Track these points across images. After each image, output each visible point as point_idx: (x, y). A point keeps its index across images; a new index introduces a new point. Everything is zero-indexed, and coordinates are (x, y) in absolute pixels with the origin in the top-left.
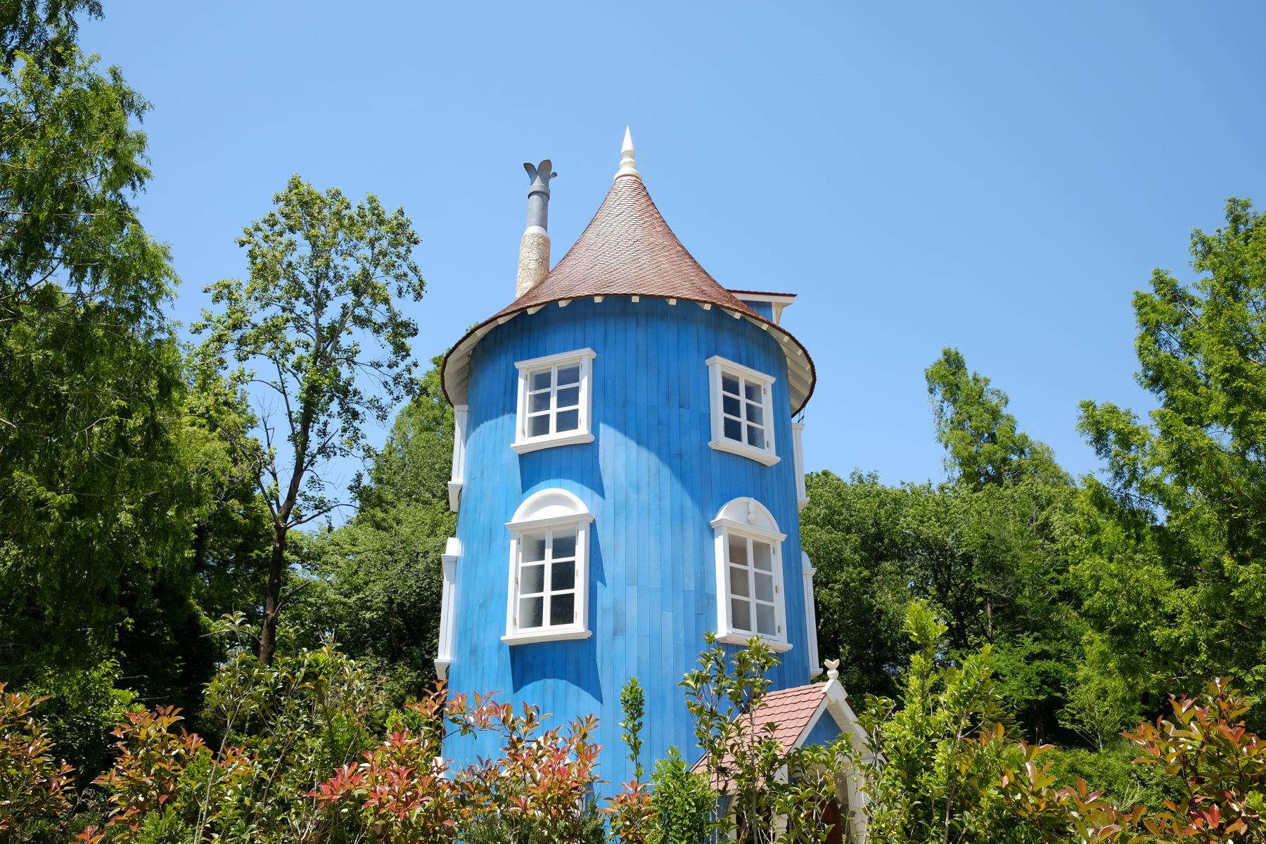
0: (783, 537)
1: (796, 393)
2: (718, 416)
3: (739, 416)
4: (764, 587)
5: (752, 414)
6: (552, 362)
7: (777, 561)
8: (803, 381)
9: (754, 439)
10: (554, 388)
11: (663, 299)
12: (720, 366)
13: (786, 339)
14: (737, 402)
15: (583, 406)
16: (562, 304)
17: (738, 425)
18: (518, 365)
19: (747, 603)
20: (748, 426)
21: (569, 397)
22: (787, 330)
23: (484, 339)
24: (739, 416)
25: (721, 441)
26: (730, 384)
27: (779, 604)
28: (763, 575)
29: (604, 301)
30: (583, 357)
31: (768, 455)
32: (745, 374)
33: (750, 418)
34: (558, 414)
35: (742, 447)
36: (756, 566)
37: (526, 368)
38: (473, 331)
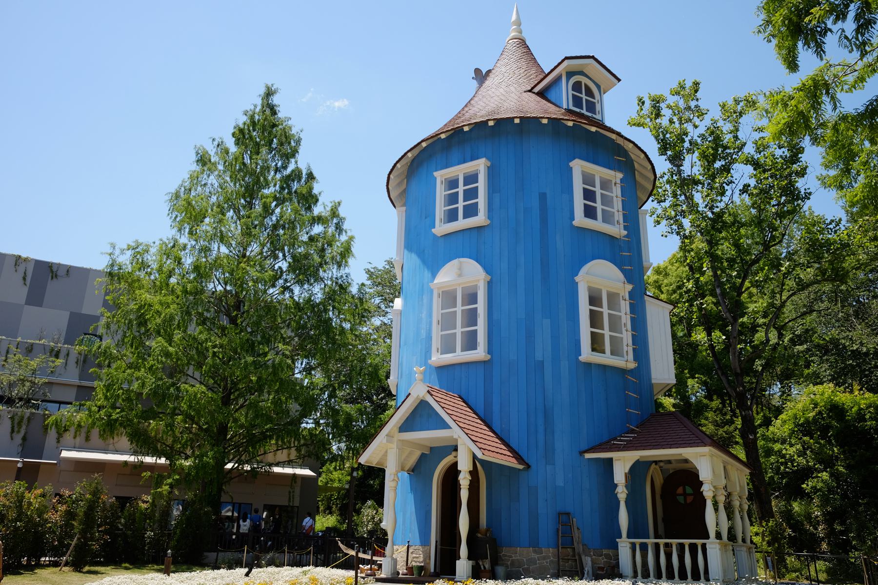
0: (629, 287)
1: (643, 188)
2: (579, 203)
3: (595, 202)
4: (615, 325)
5: (606, 201)
6: (459, 171)
7: (625, 306)
8: (646, 178)
9: (608, 218)
10: (461, 189)
11: (537, 119)
12: (578, 166)
13: (631, 145)
14: (594, 192)
15: (482, 200)
16: (466, 129)
17: (594, 209)
18: (436, 174)
19: (602, 313)
20: (601, 194)
21: (471, 194)
22: (632, 140)
23: (413, 161)
24: (595, 202)
25: (580, 220)
26: (588, 179)
27: (626, 337)
28: (605, 195)
29: (495, 124)
30: (480, 166)
31: (617, 230)
32: (600, 172)
33: (610, 307)
34: (455, 328)
35: (597, 225)
36: (602, 204)
37: (441, 175)
38: (406, 154)
